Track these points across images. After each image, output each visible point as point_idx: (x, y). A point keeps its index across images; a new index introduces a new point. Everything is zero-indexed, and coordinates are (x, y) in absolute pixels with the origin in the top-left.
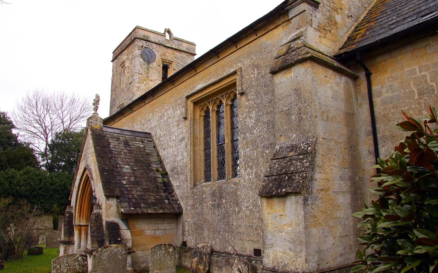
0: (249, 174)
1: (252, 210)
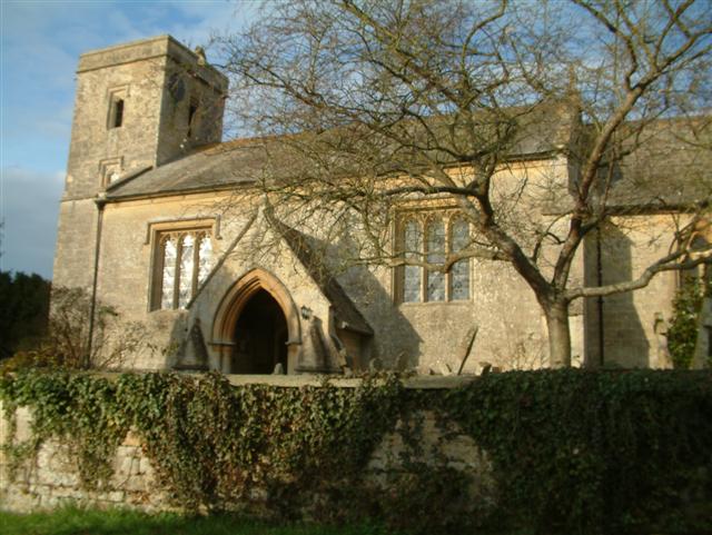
0: (489, 298)
1: (491, 332)
